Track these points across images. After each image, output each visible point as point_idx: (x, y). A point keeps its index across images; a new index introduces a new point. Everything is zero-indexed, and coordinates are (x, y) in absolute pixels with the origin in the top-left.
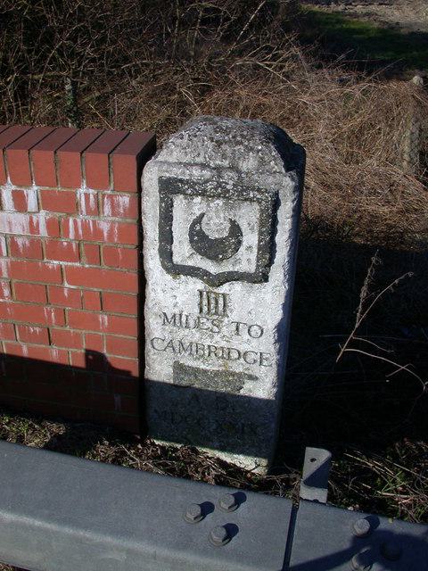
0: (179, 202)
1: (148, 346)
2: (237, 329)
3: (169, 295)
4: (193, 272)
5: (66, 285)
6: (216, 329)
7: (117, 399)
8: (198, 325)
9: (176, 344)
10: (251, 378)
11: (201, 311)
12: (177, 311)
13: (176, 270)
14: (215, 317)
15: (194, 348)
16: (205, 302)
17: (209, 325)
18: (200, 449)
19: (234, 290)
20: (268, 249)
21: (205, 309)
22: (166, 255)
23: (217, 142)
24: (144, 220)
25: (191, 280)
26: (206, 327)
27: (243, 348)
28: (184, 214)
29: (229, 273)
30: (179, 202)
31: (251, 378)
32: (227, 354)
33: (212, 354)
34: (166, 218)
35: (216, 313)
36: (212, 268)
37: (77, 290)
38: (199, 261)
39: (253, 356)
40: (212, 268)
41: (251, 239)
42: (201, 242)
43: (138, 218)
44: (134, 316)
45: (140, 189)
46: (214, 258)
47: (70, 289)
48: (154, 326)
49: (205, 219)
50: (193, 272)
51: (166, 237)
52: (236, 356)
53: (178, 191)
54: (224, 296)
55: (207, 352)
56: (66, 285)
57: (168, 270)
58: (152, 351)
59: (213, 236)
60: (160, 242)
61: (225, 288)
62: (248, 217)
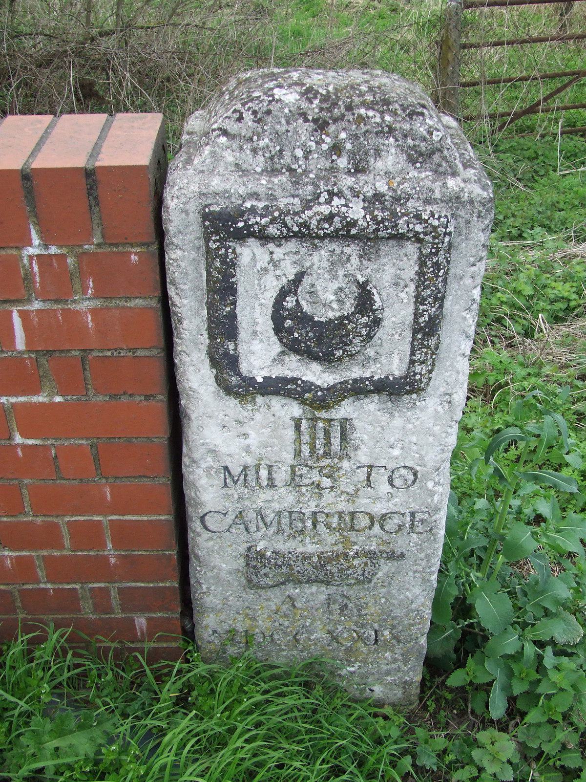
0: (249, 255)
1: (195, 525)
2: (368, 479)
3: (223, 434)
4: (276, 387)
5: (18, 439)
6: (326, 482)
7: (141, 622)
8: (294, 480)
9: (251, 515)
10: (393, 556)
11: (298, 453)
12: (250, 460)
13: (238, 386)
14: (327, 462)
15: (285, 521)
16: (306, 438)
17: (315, 477)
18: (80, 596)
19: (365, 415)
20: (426, 330)
21: (306, 450)
22: (224, 363)
23: (315, 121)
24: (171, 291)
25: (276, 402)
26: (307, 481)
27: (379, 509)
28: (260, 274)
29: (355, 381)
30: (249, 255)
31: (393, 556)
32: (348, 522)
33: (321, 527)
34: (222, 289)
35: (327, 454)
36: (317, 375)
37: (46, 448)
38: (295, 368)
39: (396, 520)
40: (317, 375)
41: (397, 311)
42: (301, 333)
43: (158, 293)
44: (165, 481)
45: (160, 234)
46: (327, 359)
47: (24, 447)
48: (206, 490)
49: (306, 281)
50: (276, 387)
51: (223, 327)
52: (366, 522)
53: (241, 236)
54: (345, 423)
55: (309, 524)
56: (18, 439)
57: (228, 390)
58: (205, 535)
59: (322, 315)
60: (212, 337)
61: (346, 409)
62: (393, 276)
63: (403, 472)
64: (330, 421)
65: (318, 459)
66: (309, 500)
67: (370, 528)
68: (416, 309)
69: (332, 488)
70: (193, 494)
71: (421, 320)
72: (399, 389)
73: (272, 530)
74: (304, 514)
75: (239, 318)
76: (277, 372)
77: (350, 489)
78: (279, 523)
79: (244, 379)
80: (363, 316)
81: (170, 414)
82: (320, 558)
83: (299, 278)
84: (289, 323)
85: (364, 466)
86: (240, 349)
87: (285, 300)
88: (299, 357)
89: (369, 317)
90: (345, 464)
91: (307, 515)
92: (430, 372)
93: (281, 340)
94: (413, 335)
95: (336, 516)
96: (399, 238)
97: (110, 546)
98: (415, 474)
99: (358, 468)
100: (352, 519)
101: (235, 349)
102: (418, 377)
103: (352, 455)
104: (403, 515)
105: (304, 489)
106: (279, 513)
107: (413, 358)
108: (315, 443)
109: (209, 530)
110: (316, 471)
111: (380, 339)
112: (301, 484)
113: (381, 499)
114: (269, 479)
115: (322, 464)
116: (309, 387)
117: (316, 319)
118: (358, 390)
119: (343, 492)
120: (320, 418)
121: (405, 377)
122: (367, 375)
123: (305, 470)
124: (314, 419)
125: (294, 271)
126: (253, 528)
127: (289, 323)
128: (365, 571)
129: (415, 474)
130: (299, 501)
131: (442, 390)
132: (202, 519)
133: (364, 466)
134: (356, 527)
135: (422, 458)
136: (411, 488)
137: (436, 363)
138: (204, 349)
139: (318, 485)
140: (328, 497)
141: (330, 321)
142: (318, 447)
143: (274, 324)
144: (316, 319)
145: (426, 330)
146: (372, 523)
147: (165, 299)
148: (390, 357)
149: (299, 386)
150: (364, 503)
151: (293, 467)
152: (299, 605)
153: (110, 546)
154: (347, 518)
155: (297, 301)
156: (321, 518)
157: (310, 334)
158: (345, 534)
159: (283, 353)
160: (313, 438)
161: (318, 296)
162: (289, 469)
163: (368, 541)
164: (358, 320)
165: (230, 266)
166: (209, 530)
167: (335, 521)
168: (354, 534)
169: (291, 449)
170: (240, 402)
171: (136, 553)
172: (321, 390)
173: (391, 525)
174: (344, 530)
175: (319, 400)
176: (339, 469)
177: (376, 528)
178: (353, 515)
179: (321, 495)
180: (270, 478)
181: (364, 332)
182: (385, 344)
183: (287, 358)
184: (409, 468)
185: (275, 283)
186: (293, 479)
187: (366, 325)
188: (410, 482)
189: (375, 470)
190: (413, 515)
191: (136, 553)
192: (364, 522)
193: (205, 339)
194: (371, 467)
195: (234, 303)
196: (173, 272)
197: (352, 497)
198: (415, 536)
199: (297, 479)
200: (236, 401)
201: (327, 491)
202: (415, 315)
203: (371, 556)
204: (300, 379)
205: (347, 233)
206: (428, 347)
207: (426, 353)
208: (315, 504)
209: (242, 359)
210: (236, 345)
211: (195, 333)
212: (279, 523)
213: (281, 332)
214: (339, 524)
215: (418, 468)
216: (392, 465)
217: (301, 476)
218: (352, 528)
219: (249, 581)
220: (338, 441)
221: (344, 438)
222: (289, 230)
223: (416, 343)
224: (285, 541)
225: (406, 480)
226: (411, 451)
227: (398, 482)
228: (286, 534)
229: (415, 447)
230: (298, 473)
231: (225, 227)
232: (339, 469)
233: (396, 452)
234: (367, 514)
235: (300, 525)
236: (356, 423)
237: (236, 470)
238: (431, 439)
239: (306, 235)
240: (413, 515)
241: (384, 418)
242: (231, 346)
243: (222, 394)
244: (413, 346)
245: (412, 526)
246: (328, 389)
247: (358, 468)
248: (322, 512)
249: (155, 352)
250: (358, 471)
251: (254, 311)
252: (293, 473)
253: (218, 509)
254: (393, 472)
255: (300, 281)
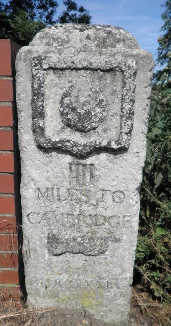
6: (84, 198)
12: (49, 185)
22: (38, 131)
27: (108, 213)
34: (38, 94)
51: (39, 114)
70: (25, 203)
79: (47, 140)
81: (14, 134)
110: (79, 192)
115: (82, 188)
118: (98, 150)
119: (91, 204)
131: (135, 150)
147: (14, 102)
150: (101, 210)
159: (63, 128)
173: (114, 221)
185: (61, 92)
195: (43, 101)
196: (18, 91)
197: (96, 206)
209: (46, 129)
216: (113, 190)
227: (117, 200)
233: (115, 183)
237: (43, 190)
238: (131, 176)
241: (110, 164)
245: (123, 224)
251: (52, 109)
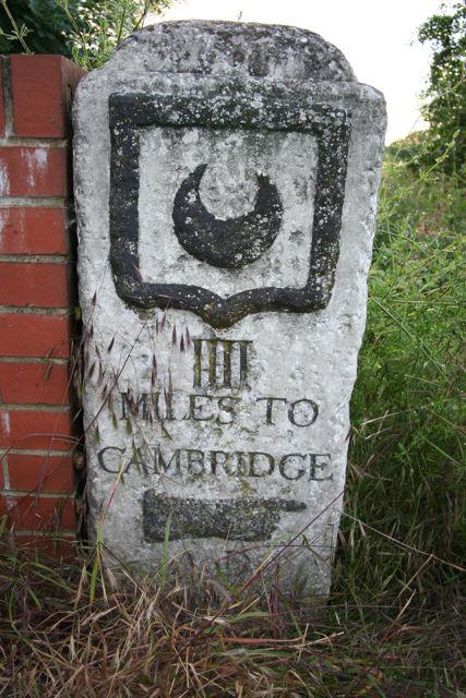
0: (153, 147)
2: (269, 415)
6: (226, 416)
10: (293, 507)
11: (197, 383)
13: (142, 298)
14: (226, 392)
15: (184, 462)
20: (326, 236)
21: (205, 377)
22: (123, 265)
27: (278, 450)
28: (160, 166)
30: (153, 147)
31: (293, 507)
32: (247, 465)
33: (220, 469)
34: (125, 182)
35: (227, 384)
36: (219, 284)
40: (219, 284)
41: (298, 215)
42: (204, 237)
46: (225, 263)
51: (124, 226)
55: (208, 466)
59: (224, 213)
61: (245, 329)
62: (293, 164)
63: (304, 406)
64: (229, 343)
65: (217, 388)
66: (208, 437)
67: (270, 472)
68: (316, 211)
69: (232, 422)
71: (321, 222)
72: (301, 303)
73: (173, 470)
74: (203, 454)
75: (141, 216)
76: (174, 278)
77: (250, 425)
78: (178, 465)
80: (263, 217)
82: (218, 506)
83: (199, 172)
84: (189, 220)
85: (265, 399)
86: (140, 250)
87: (186, 195)
88: (199, 263)
89: (269, 217)
90: (245, 395)
91: (206, 456)
92: (330, 287)
93: (181, 242)
94: (313, 240)
95: (236, 458)
96: (298, 128)
97: (7, 487)
98: (316, 410)
99: (258, 400)
100: (252, 462)
101: (136, 251)
102: (318, 289)
103: (252, 385)
104: (304, 457)
105: (203, 424)
106: (178, 452)
107: (315, 267)
108: (215, 370)
109: (106, 470)
111: (280, 244)
112: (200, 417)
113: (281, 440)
114: (168, 411)
116: (208, 296)
117: (217, 218)
119: (243, 429)
120: (219, 339)
121: (306, 289)
122: (269, 285)
123: (204, 401)
124: (214, 341)
125: (196, 164)
126: (151, 471)
127: (189, 220)
128: (264, 522)
129: (316, 410)
130: (198, 439)
132: (100, 456)
133: (265, 399)
134: (257, 472)
135: (322, 391)
136: (312, 426)
137: (336, 278)
138: (106, 253)
139: (218, 420)
140: (228, 433)
141: (230, 221)
142: (218, 374)
143: (175, 222)
144: (217, 218)
145: (326, 236)
146: (272, 469)
148: (286, 263)
149: (198, 295)
151: (192, 397)
152: (197, 563)
153: (7, 487)
154: (247, 460)
155: (198, 197)
156: (221, 459)
157: (211, 234)
158: (244, 478)
160: (214, 363)
161: (218, 193)
162: (188, 399)
163: (268, 489)
164: (258, 220)
165: (133, 154)
166: (106, 470)
167: (234, 463)
168: (253, 479)
169: (191, 375)
170: (141, 317)
171: (29, 452)
172: (222, 301)
174: (243, 475)
175: (221, 315)
176: (239, 400)
177: (277, 474)
178: (252, 455)
179: (220, 433)
180: (170, 411)
181: (265, 233)
182: (285, 251)
183: (186, 263)
184: (309, 401)
186: (193, 412)
187: (265, 226)
188: (310, 418)
189: (275, 403)
190: (313, 457)
191: (29, 452)
192: (264, 465)
193: (107, 243)
194: (271, 400)
195: (136, 197)
196: (78, 165)
197: (252, 434)
198: (315, 483)
199: (196, 412)
200: (136, 316)
201: (227, 426)
202: (315, 217)
203: (271, 505)
204: (200, 288)
205: (246, 123)
206: (328, 255)
207: (326, 262)
208: (214, 441)
210: (136, 246)
211: (97, 236)
212: (178, 465)
213: (182, 231)
214: (239, 468)
215: (318, 402)
216: (292, 398)
217: (200, 408)
218: (252, 474)
219: (146, 532)
220: (238, 366)
221: (244, 366)
222: (191, 115)
223: (316, 250)
224: (183, 485)
225: (306, 416)
226: (310, 372)
227: (298, 418)
228: (184, 477)
229: (316, 377)
230: (197, 404)
231: (131, 115)
232: (239, 400)
234: (268, 455)
235: (199, 467)
236: (256, 346)
239: (207, 123)
240: (313, 457)
242: (132, 247)
243: (123, 306)
244: (312, 252)
246: (229, 300)
247: (258, 400)
248: (222, 452)
249: (59, 260)
250: (258, 404)
251: (154, 213)
252: (193, 405)
253: (116, 446)
254: (293, 405)
255: (202, 175)
